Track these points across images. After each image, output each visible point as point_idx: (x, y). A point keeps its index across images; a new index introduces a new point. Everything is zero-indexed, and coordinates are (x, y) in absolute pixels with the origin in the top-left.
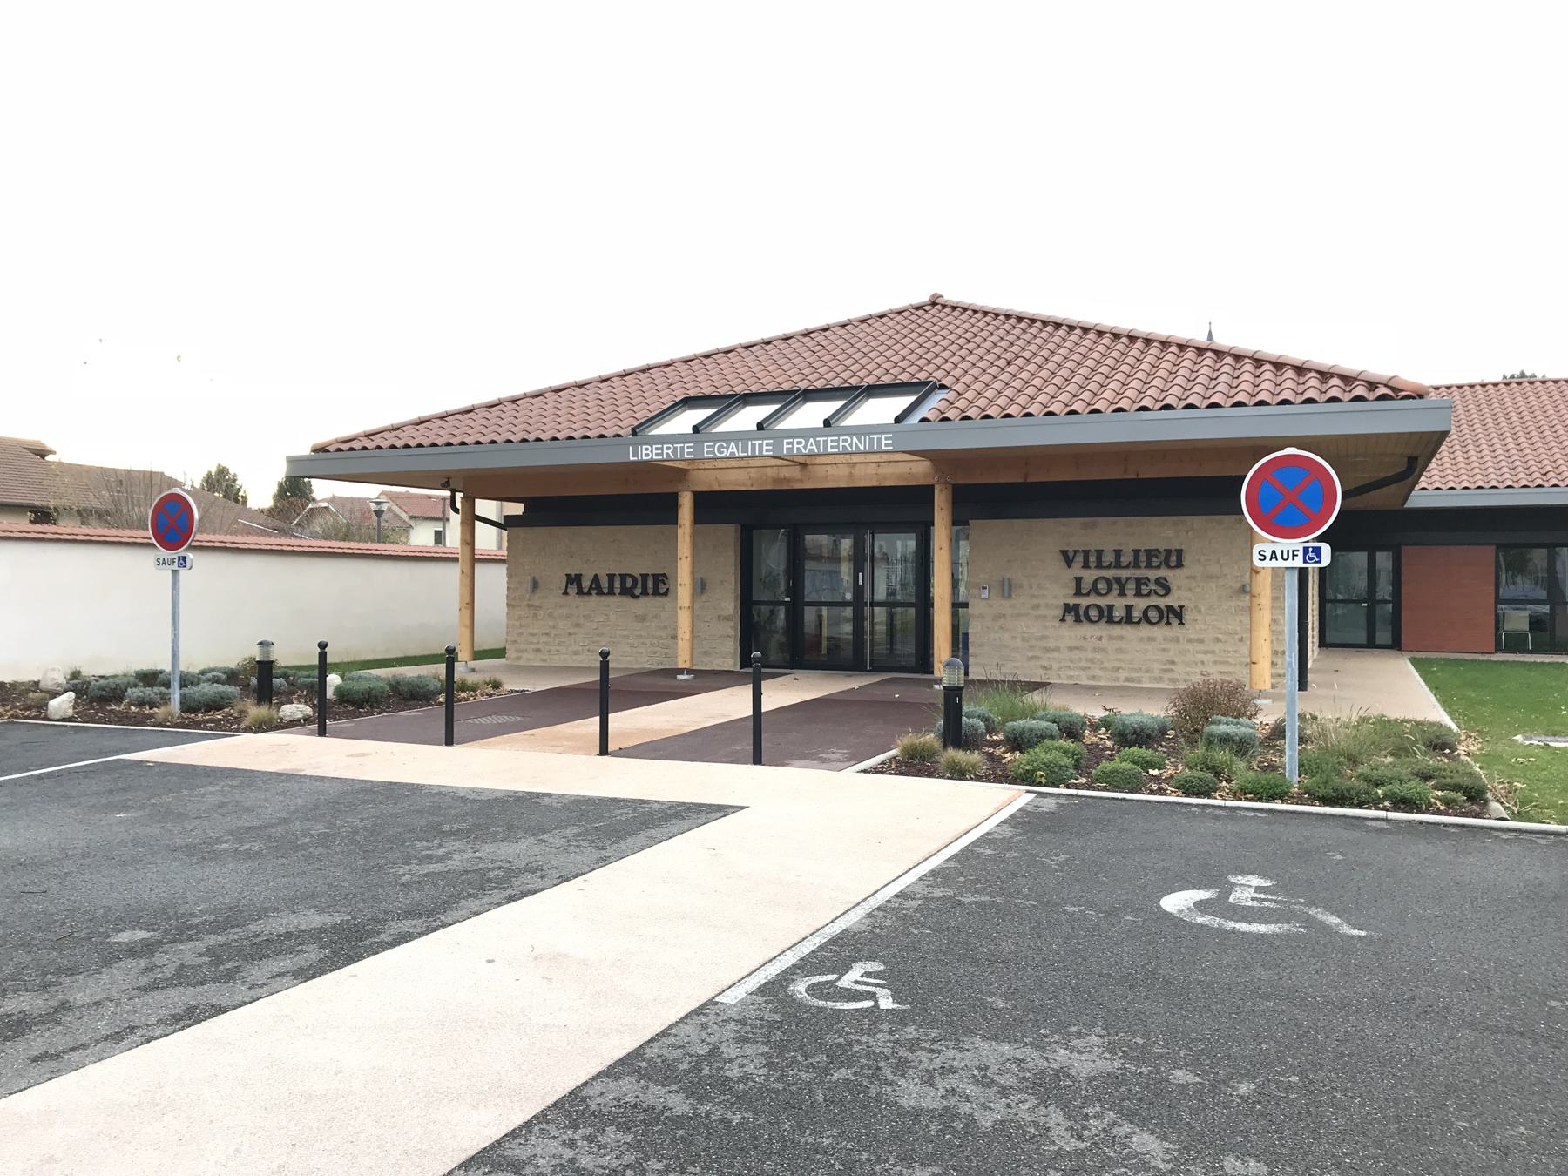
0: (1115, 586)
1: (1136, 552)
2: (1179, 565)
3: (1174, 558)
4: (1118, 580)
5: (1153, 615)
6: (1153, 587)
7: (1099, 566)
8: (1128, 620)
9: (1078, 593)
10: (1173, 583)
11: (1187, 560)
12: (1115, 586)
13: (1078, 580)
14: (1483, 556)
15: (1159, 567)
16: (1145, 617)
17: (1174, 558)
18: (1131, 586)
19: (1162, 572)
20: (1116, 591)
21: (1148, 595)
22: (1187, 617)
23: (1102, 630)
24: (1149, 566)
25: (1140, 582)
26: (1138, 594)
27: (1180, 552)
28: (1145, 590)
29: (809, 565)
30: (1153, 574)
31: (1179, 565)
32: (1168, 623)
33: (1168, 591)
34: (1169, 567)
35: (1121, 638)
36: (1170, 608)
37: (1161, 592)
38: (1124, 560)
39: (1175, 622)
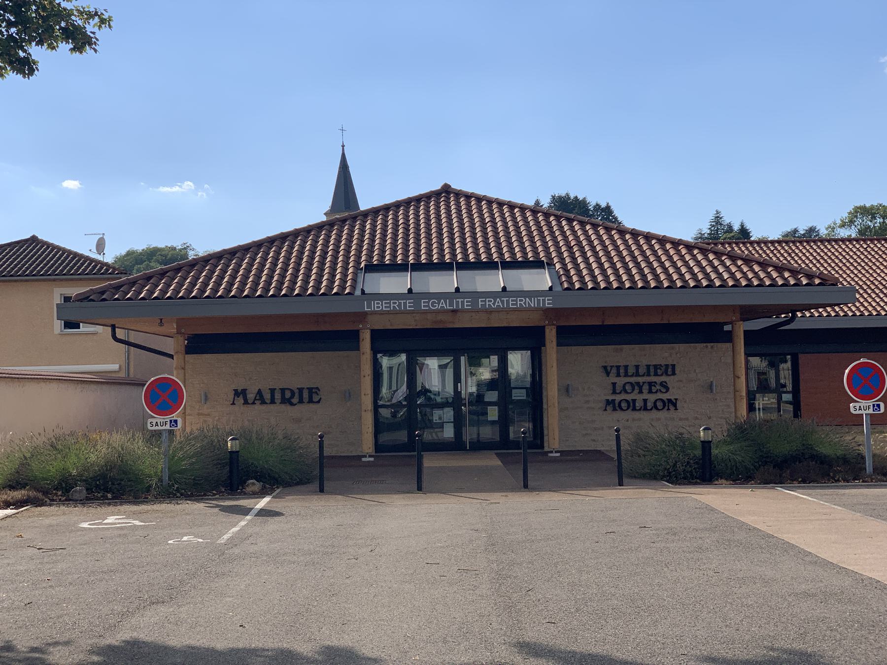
1: (648, 366)
2: (674, 374)
6: (658, 387)
7: (626, 375)
13: (614, 384)
15: (662, 375)
16: (655, 407)
17: (670, 370)
18: (645, 388)
19: (663, 378)
21: (656, 392)
23: (629, 414)
27: (673, 366)
28: (654, 389)
31: (674, 374)
33: (667, 389)
34: (667, 375)
36: (670, 401)
37: (664, 390)
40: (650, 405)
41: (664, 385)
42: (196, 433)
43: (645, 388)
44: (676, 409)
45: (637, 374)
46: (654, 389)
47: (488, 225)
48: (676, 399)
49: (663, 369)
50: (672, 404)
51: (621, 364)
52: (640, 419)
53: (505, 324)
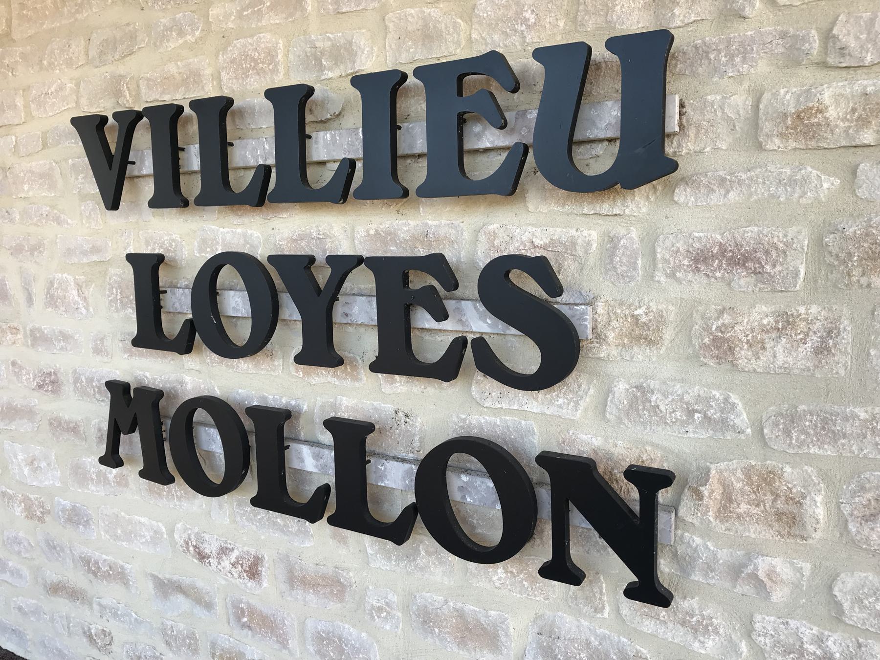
0: (290, 311)
1: (381, 92)
2: (646, 160)
3: (605, 116)
4: (295, 267)
5: (475, 495)
6: (474, 320)
7: (219, 192)
8: (349, 505)
9: (150, 335)
10: (596, 300)
11: (706, 112)
12: (290, 311)
13: (148, 269)
14: (606, 143)
15: (507, 185)
16: (433, 514)
17: (605, 116)
18: (358, 314)
19: (534, 224)
20: (290, 336)
21: (446, 369)
22: (690, 535)
23: (233, 519)
24: (451, 180)
25: (408, 285)
26: (396, 357)
27: (647, 57)
28: (432, 336)
29: (182, 178)
30: (468, 233)
31: (646, 160)
32: (563, 570)
33: (561, 353)
34: (575, 183)
35: (333, 585)
36: (576, 479)
37: (526, 356)
38: (335, 143)
39: (611, 571)
40: (393, 482)
41: (526, 294)
42: (676, 451)
43: (358, 314)
44: (648, 591)
45: (288, 182)
46: (432, 336)
47: (855, 258)
48: (651, 480)
49: (526, 110)
50: (604, 518)
51: (181, 97)
52: (333, 585)
53: (274, 140)
